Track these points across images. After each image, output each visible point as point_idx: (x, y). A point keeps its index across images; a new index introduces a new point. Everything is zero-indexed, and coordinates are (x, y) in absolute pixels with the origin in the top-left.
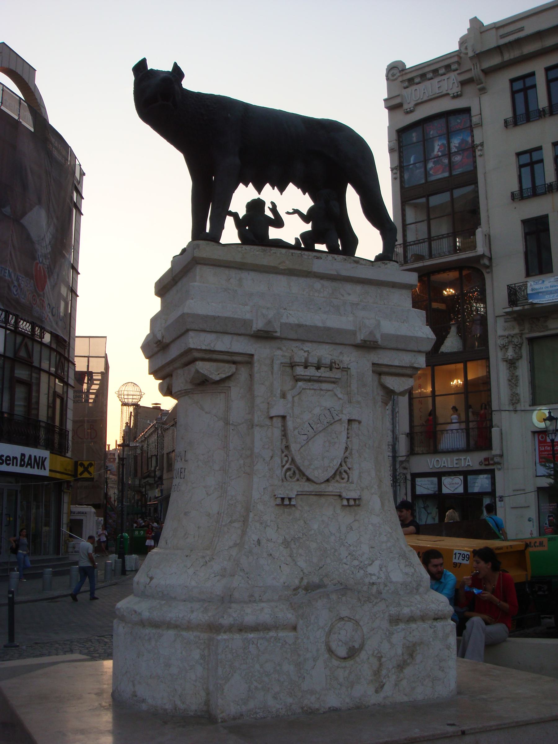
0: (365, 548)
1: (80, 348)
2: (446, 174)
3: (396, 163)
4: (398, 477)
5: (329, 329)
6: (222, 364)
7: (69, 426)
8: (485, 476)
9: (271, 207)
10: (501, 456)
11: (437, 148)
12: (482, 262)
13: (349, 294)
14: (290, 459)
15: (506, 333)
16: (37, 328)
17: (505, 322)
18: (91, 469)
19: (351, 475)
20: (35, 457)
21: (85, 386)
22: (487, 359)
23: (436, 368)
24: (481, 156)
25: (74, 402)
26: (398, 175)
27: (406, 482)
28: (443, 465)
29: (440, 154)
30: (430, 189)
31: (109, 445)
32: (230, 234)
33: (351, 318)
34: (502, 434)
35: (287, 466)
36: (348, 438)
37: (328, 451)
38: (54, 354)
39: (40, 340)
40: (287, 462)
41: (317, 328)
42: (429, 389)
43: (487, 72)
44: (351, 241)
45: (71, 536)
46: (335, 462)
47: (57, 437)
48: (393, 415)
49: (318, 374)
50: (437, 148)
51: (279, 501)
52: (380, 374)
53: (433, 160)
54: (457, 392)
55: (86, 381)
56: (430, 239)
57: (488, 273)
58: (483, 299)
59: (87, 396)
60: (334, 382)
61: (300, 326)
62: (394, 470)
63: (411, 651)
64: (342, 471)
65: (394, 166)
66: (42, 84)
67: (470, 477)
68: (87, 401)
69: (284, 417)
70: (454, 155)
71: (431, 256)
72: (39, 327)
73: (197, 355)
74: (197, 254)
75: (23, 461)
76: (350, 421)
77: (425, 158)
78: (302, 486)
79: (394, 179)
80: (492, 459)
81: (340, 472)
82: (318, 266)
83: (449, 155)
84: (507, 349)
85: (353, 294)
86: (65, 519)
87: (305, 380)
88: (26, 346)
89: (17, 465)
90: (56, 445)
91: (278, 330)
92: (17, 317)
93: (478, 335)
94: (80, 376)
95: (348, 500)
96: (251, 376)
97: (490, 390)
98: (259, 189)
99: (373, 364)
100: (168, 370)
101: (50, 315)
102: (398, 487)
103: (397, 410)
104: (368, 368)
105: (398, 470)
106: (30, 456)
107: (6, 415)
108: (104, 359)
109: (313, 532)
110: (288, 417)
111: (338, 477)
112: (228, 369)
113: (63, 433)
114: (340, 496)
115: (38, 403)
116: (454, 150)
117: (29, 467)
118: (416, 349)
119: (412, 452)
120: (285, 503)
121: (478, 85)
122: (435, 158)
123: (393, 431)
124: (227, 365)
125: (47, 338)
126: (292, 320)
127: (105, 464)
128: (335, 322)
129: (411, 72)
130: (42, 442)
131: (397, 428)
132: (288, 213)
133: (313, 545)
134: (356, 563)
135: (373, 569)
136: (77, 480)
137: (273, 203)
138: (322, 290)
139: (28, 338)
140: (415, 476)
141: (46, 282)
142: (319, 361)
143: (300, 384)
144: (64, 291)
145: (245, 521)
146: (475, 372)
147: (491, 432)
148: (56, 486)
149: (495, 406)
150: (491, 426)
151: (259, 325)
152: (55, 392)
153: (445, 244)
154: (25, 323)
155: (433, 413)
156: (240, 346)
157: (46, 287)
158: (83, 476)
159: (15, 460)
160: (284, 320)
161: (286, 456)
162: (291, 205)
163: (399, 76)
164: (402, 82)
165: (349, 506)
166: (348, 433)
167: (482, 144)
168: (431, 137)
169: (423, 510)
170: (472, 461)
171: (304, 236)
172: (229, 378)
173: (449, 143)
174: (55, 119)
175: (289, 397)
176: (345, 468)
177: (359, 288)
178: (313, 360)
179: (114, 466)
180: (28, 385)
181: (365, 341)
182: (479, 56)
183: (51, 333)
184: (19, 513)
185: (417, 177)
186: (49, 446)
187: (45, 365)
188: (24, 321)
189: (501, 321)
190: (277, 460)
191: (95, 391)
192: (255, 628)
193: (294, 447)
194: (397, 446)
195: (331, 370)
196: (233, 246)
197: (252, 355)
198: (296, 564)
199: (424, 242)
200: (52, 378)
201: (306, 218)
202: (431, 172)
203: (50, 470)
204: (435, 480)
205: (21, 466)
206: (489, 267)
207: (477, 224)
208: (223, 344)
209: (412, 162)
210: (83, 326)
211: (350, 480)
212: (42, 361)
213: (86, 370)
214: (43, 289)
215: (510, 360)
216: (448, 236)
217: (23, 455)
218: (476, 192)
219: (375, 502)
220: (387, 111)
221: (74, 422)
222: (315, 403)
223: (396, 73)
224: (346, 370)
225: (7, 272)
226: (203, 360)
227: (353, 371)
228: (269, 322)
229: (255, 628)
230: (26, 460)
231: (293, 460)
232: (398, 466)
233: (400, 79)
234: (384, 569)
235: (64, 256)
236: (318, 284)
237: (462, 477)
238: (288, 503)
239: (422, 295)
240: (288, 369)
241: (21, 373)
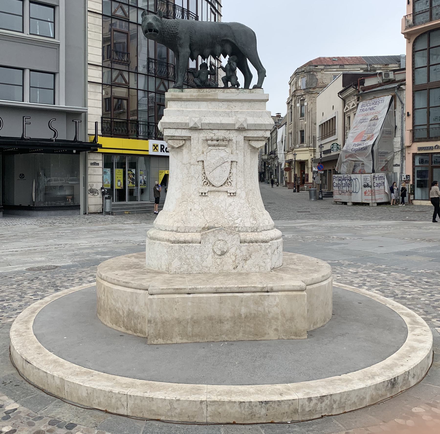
0: (236, 213)
5: (222, 124)
33: (234, 118)
35: (204, 180)
41: (218, 124)
69: (203, 161)
76: (232, 162)
95: (230, 193)
104: (243, 138)
111: (226, 184)
112: (182, 143)
120: (203, 194)
134: (231, 218)
135: (238, 221)
151: (191, 125)
175: (205, 153)
176: (229, 180)
177: (240, 104)
178: (215, 138)
190: (200, 178)
192: (185, 242)
198: (205, 219)
208: (178, 133)
227: (234, 141)
228: (195, 123)
229: (185, 242)
234: (242, 221)
236: (221, 104)
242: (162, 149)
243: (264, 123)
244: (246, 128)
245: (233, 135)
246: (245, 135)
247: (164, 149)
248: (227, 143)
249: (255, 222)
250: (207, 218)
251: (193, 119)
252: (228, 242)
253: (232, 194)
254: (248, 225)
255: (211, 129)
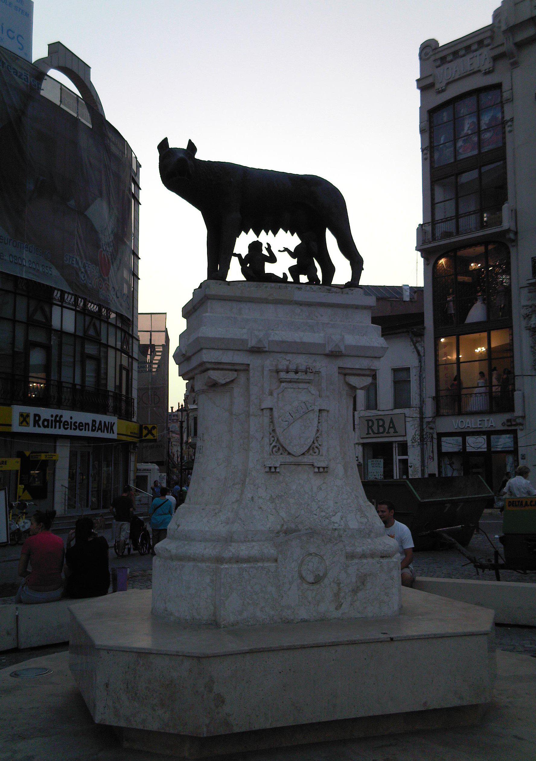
0: (331, 503)
1: (142, 324)
2: (475, 152)
3: (427, 144)
4: (425, 436)
5: (304, 343)
6: (227, 372)
7: (135, 394)
8: (508, 436)
9: (267, 247)
10: (524, 417)
11: (467, 126)
12: (507, 236)
13: (322, 316)
14: (276, 439)
15: (530, 303)
16: (103, 309)
17: (529, 292)
18: (154, 432)
19: (321, 450)
20: (105, 422)
21: (149, 357)
22: (511, 327)
23: (461, 337)
24: (510, 131)
25: (139, 372)
26: (428, 155)
27: (432, 441)
28: (467, 425)
29: (470, 132)
30: (458, 168)
31: (172, 408)
32: (235, 273)
33: (322, 335)
34: (524, 397)
35: (274, 444)
36: (319, 423)
37: (303, 433)
38: (119, 334)
39: (106, 320)
40: (274, 441)
41: (295, 342)
42: (455, 357)
43: (520, 45)
44: (329, 270)
45: (137, 491)
46: (309, 440)
47: (123, 405)
48: (420, 380)
49: (296, 377)
50: (466, 128)
51: (267, 469)
52: (345, 375)
53: (463, 138)
54: (481, 359)
55: (149, 353)
56: (457, 216)
57: (514, 246)
58: (507, 271)
59: (151, 366)
60: (308, 383)
61: (282, 342)
62: (422, 430)
63: (363, 579)
64: (315, 447)
65: (424, 147)
66: (97, 80)
67: (493, 437)
68: (151, 371)
69: (271, 409)
70: (484, 133)
71: (458, 233)
72: (106, 308)
73: (209, 366)
74: (208, 292)
75: (94, 426)
77: (455, 136)
78: (283, 459)
79: (424, 159)
80: (515, 420)
81: (313, 448)
82: (299, 296)
83: (479, 132)
84: (531, 318)
85: (325, 316)
86: (132, 476)
87: (287, 382)
88: (94, 325)
89: (89, 430)
90: (123, 412)
91: (266, 345)
92: (85, 300)
93: (502, 305)
94: (144, 349)
95: (319, 468)
96: (248, 379)
97: (512, 357)
98: (258, 234)
99: (339, 368)
100: (191, 375)
101: (115, 297)
102: (425, 446)
103: (424, 375)
104: (336, 370)
105: (425, 430)
106: (100, 422)
107: (78, 387)
108: (164, 333)
109: (292, 491)
110: (274, 409)
111: (311, 452)
112: (231, 375)
113: (129, 401)
114: (313, 465)
115: (106, 374)
116: (483, 127)
117: (100, 431)
118: (372, 355)
119: (438, 414)
120: (272, 471)
121: (510, 59)
122: (464, 137)
123: (421, 395)
124: (230, 372)
125: (113, 315)
126: (277, 338)
127: (167, 426)
128: (308, 337)
129: (442, 51)
130: (111, 409)
131: (424, 392)
132: (279, 251)
133: (292, 501)
134: (323, 514)
136: (141, 441)
137: (268, 244)
138: (301, 314)
139: (96, 318)
140: (440, 435)
141: (110, 267)
142: (297, 368)
143: (283, 384)
144: (126, 274)
145: (243, 483)
146: (498, 339)
147: (513, 395)
148: (124, 448)
149: (517, 372)
150: (514, 390)
151: (252, 343)
152: (121, 365)
153: (473, 220)
154: (93, 305)
155: (458, 378)
156: (240, 358)
157: (110, 273)
158: (146, 438)
159: (87, 426)
160: (272, 338)
161: (273, 437)
162: (282, 243)
163: (431, 55)
164: (435, 60)
165: (319, 472)
166: (319, 419)
167: (512, 120)
168: (462, 115)
169: (449, 466)
170: (496, 421)
171: (291, 269)
172: (232, 381)
173: (479, 120)
174: (112, 116)
175: (275, 395)
176: (316, 444)
177: (329, 311)
178: (293, 367)
179: (175, 426)
180: (97, 360)
181: (332, 352)
182: (512, 29)
183: (116, 313)
184: (91, 472)
185: (446, 156)
186: (116, 412)
187: (112, 342)
188: (92, 303)
189: (525, 291)
190: (266, 440)
191: (157, 362)
193: (279, 430)
194: (424, 408)
195: (306, 374)
196: (236, 283)
197: (249, 365)
199: (452, 220)
200: (119, 353)
201: (293, 255)
202: (460, 151)
203: (118, 434)
204: (460, 439)
205: (93, 430)
206: (514, 241)
207: (505, 199)
208: (227, 358)
209: (442, 142)
210: (143, 306)
211: (321, 452)
212: (109, 336)
213: (149, 343)
214: (107, 275)
215: (533, 328)
216: (475, 212)
217: (94, 421)
218: (505, 167)
219: (340, 470)
220: (418, 92)
221: (139, 390)
222: (295, 398)
223: (430, 51)
224: (318, 373)
225: (75, 260)
226: (214, 369)
228: (260, 341)
230: (97, 425)
231: (278, 439)
232: (425, 426)
233: (433, 58)
234: (344, 519)
235: (124, 243)
236: (298, 310)
237: (485, 437)
238: (274, 470)
239: (448, 269)
240: (275, 374)
241: (90, 349)
242: (36, 423)
243: (372, 345)
244: (344, 352)
245: (322, 365)
246: (342, 365)
247: (40, 422)
248: (312, 378)
249: (364, 520)
250: (283, 514)
251: (256, 333)
252: (324, 558)
253: (321, 470)
254: (353, 525)
255: (284, 352)
